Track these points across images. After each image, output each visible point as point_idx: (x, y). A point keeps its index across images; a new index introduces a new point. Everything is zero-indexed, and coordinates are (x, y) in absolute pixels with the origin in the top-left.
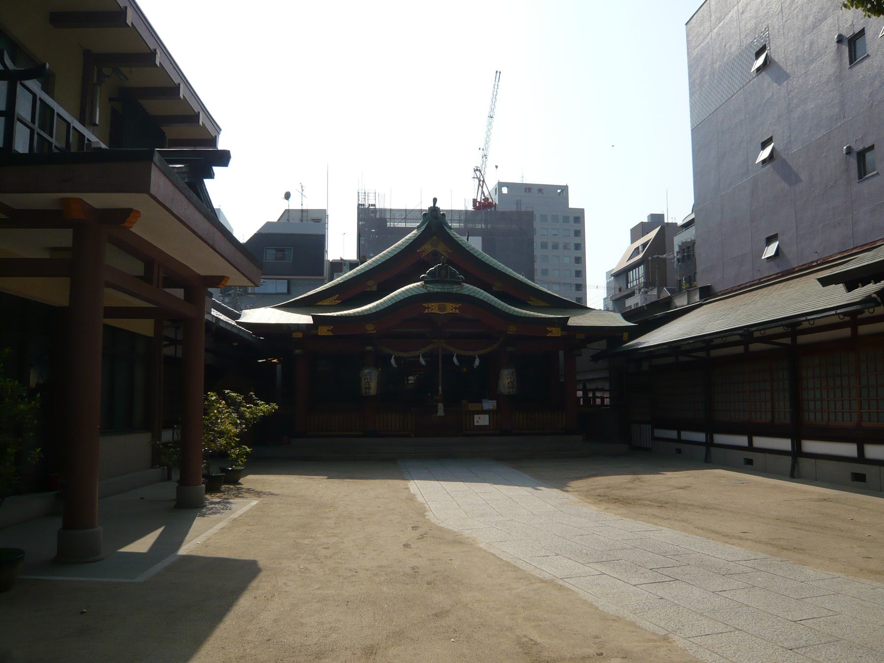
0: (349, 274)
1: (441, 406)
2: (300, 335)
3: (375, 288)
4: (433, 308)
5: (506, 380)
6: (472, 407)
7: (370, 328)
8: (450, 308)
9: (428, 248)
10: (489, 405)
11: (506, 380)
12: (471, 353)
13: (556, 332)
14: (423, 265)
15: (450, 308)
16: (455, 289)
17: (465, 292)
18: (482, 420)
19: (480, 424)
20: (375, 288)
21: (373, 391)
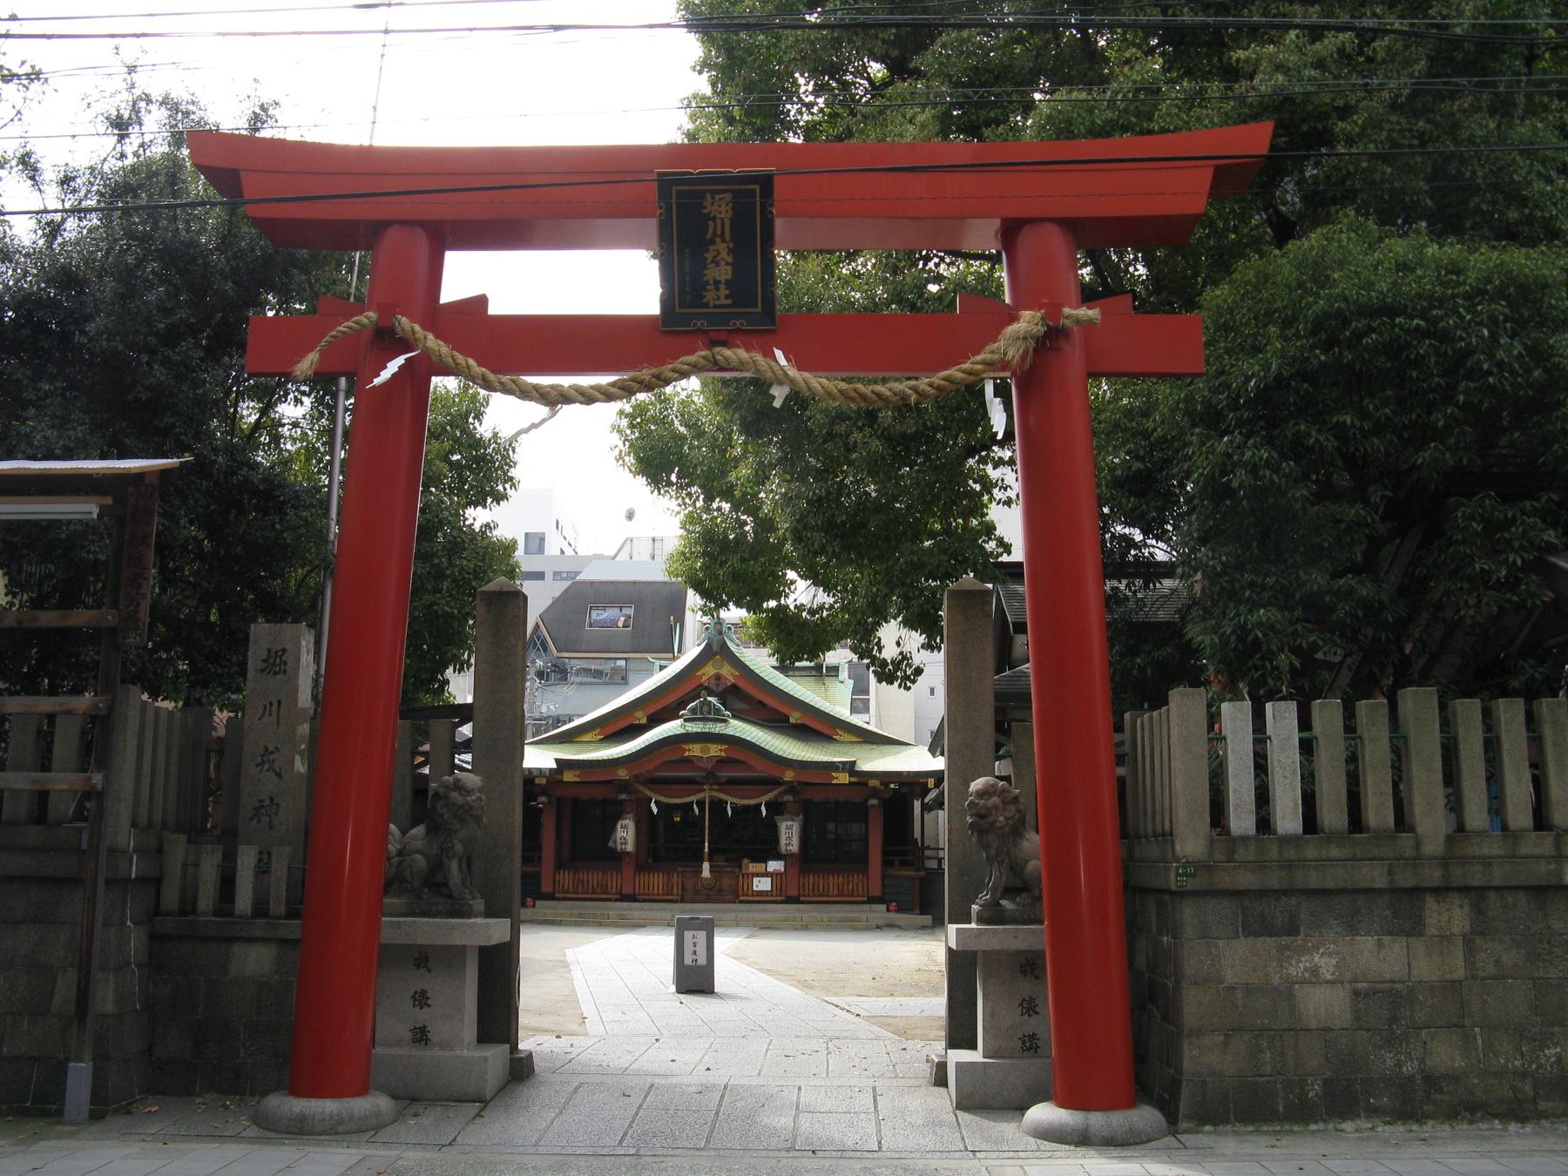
0: (862, 375)
1: (706, 866)
2: (544, 781)
3: (644, 721)
4: (695, 750)
5: (789, 834)
6: (753, 867)
7: (623, 774)
8: (715, 750)
9: (709, 671)
10: (774, 866)
11: (789, 834)
12: (687, 800)
13: (843, 778)
14: (682, 704)
15: (715, 750)
16: (718, 728)
17: (729, 731)
18: (762, 884)
19: (761, 888)
20: (644, 721)
21: (630, 848)
